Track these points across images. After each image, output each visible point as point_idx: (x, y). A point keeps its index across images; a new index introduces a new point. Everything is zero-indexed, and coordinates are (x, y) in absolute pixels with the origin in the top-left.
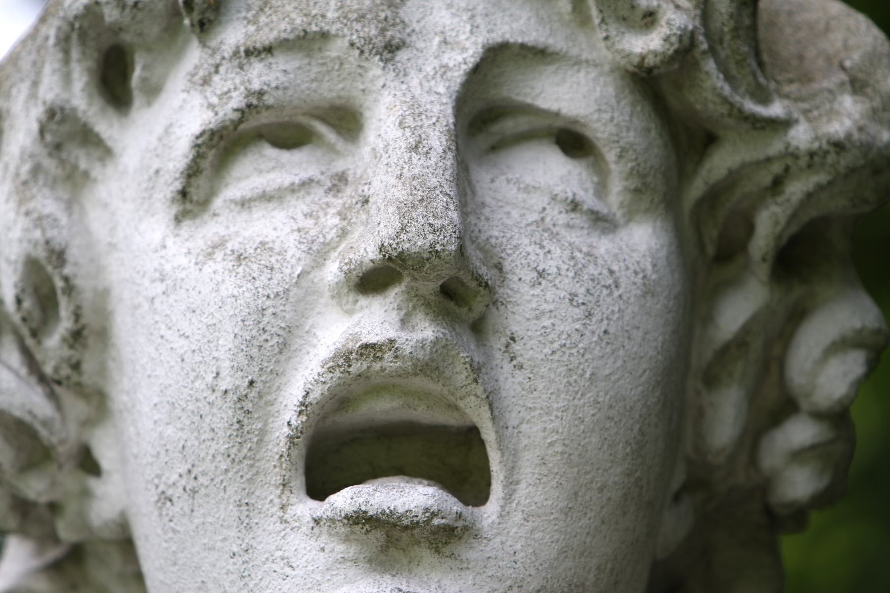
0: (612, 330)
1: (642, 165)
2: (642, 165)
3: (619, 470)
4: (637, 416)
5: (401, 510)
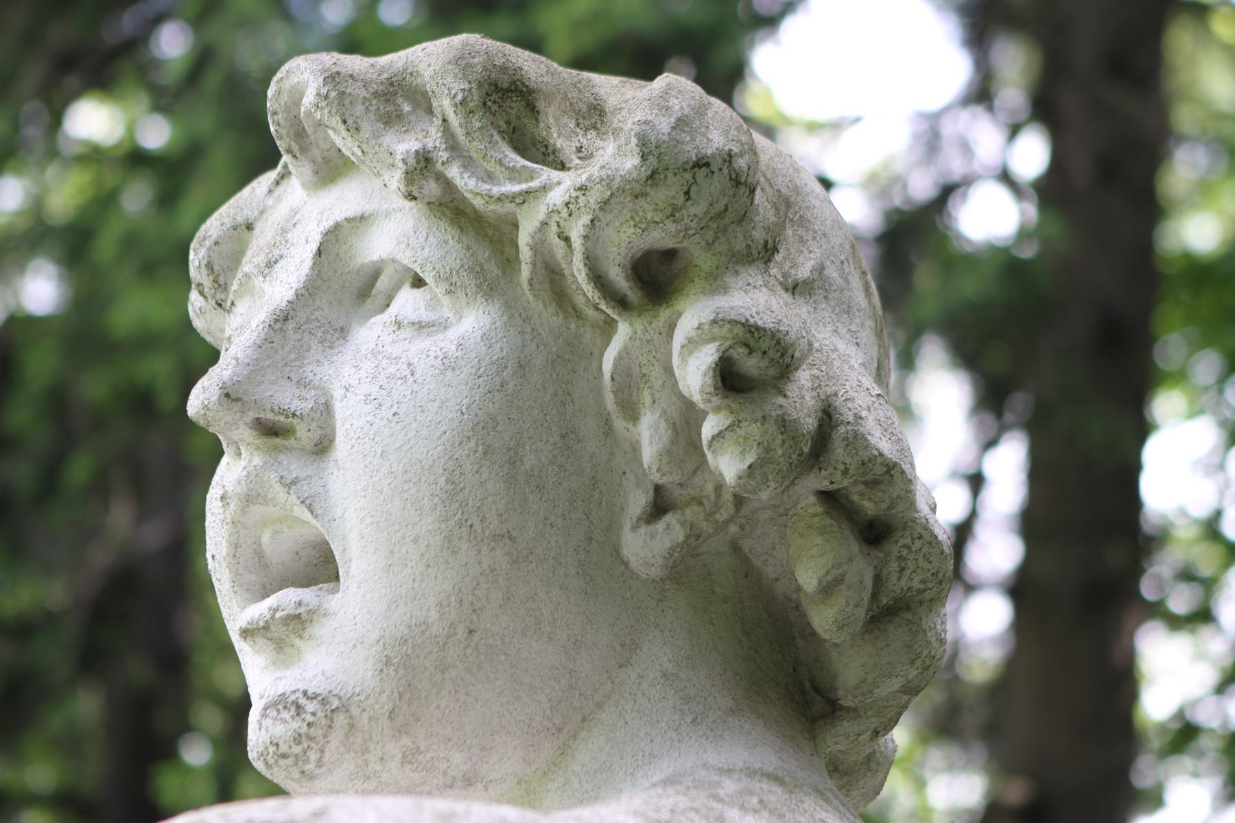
0: (401, 411)
1: (442, 271)
2: (442, 271)
3: (430, 520)
4: (441, 471)
5: (257, 616)
